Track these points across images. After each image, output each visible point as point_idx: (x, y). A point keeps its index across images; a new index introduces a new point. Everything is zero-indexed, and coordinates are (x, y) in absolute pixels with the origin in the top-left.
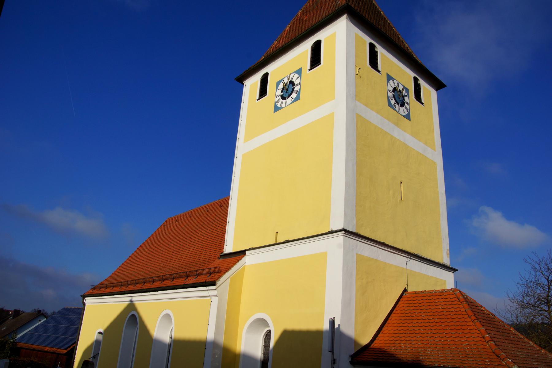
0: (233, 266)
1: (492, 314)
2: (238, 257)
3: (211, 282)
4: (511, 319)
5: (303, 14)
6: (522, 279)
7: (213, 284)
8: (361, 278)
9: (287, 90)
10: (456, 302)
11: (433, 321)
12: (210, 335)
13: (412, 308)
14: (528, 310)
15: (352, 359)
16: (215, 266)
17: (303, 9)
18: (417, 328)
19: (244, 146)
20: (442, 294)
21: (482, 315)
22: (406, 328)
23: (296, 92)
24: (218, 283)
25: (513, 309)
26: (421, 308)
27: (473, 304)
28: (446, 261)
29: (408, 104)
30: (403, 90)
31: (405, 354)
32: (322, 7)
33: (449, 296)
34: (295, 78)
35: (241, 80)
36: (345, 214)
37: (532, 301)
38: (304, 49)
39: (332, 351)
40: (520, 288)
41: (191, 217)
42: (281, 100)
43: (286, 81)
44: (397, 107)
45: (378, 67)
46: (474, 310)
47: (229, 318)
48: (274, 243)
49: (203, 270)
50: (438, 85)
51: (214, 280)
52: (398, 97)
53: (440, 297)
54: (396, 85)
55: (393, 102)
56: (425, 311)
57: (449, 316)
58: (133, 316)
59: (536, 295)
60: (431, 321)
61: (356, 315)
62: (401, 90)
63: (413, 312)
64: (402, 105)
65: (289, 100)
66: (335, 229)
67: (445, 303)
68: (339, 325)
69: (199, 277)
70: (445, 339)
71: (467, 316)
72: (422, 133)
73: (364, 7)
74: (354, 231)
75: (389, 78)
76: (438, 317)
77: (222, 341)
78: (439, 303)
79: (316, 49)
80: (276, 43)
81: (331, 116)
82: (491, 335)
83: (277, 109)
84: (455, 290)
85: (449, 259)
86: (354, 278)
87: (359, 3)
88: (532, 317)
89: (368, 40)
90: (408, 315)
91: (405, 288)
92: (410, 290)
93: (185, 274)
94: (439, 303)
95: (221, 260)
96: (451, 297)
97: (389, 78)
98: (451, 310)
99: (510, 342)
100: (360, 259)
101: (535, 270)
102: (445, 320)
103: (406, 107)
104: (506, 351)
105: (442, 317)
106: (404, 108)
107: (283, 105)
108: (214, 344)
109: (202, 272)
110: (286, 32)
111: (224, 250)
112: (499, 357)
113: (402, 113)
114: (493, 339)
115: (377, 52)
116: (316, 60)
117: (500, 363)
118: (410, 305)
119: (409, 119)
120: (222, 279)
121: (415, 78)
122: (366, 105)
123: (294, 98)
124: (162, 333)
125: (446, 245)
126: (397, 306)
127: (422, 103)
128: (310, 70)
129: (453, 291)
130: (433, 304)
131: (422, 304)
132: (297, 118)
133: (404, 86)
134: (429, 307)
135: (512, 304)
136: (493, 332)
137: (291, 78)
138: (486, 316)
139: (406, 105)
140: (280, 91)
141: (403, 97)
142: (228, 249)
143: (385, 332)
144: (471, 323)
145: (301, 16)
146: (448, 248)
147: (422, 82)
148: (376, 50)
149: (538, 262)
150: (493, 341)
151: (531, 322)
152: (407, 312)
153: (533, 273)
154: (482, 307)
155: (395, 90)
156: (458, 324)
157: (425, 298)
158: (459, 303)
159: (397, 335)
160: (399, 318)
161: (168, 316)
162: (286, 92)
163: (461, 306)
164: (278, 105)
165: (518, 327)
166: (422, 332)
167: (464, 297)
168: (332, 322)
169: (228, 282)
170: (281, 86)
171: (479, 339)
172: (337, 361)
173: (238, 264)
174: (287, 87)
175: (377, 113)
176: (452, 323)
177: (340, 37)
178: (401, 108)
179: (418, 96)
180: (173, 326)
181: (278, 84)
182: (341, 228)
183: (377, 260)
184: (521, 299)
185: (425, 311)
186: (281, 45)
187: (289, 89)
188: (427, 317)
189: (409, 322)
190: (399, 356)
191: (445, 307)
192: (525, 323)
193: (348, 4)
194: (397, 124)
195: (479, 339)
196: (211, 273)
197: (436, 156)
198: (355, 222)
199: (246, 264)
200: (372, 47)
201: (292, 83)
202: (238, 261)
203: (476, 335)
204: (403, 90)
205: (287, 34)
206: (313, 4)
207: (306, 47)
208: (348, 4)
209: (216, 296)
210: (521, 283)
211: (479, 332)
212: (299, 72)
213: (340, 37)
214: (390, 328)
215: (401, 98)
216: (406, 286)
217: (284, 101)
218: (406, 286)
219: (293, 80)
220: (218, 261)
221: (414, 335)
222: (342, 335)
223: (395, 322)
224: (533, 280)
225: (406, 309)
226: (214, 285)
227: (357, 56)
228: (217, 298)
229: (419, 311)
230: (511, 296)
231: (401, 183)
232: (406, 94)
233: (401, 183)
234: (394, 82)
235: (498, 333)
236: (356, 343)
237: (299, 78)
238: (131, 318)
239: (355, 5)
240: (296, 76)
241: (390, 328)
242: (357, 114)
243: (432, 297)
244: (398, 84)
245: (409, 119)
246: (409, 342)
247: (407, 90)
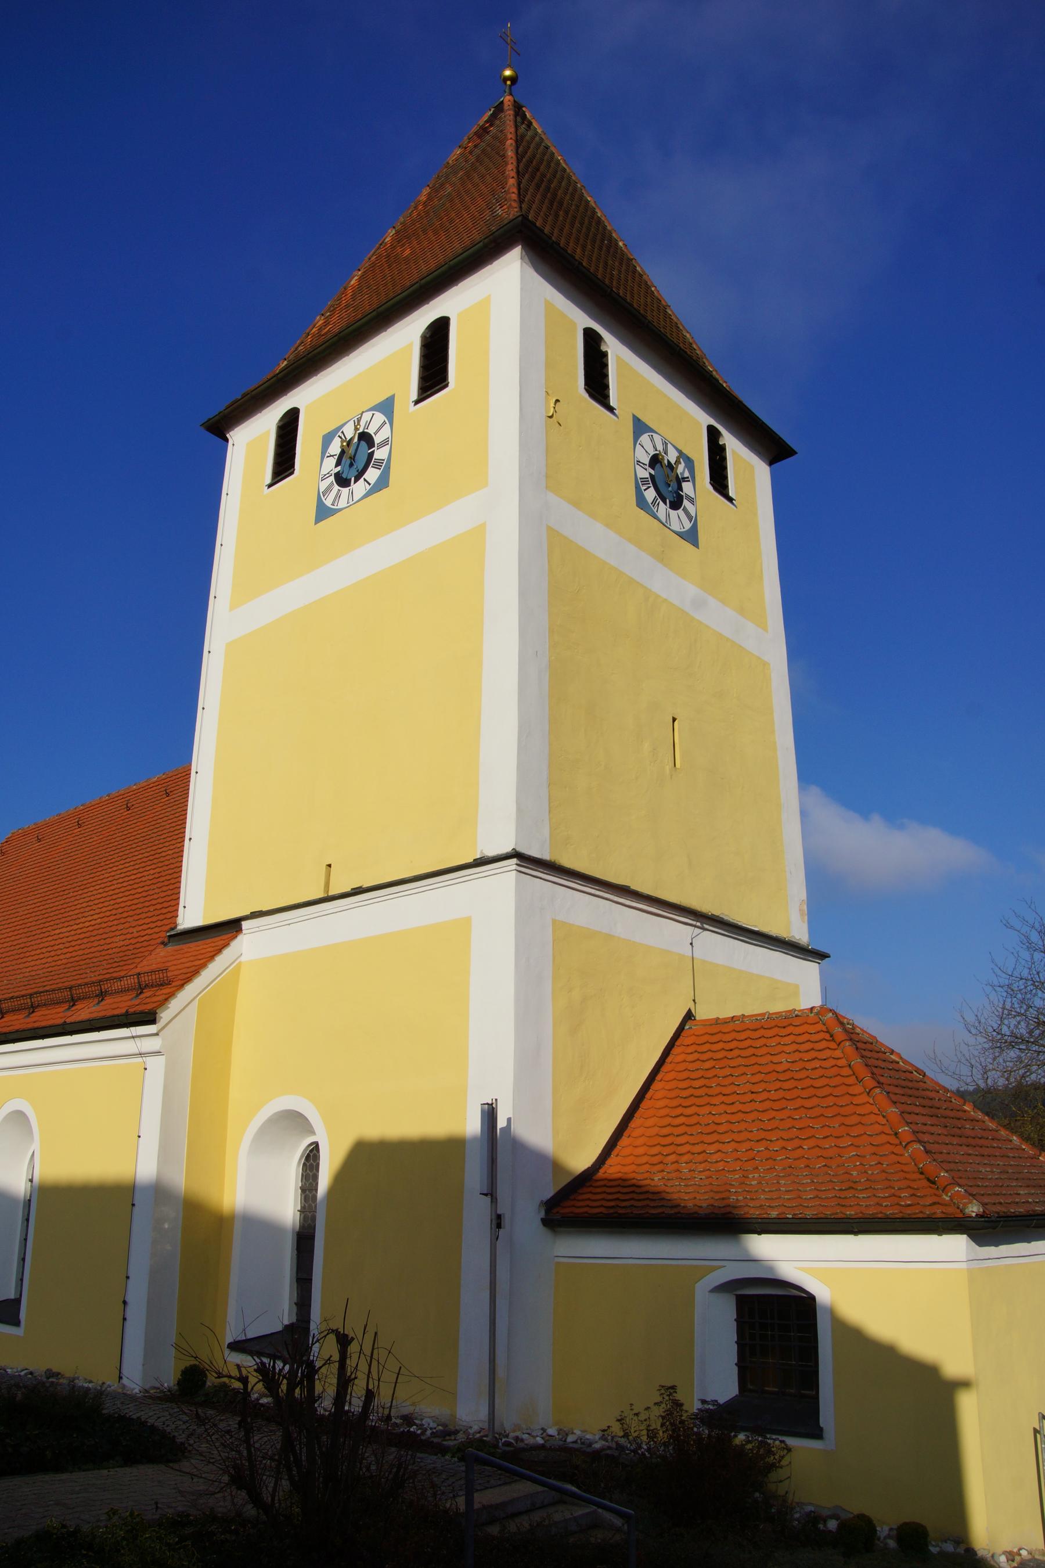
0: (204, 966)
1: (918, 1070)
2: (218, 941)
3: (142, 1013)
4: (969, 1080)
5: (403, 236)
6: (999, 973)
7: (149, 1018)
8: (566, 987)
9: (353, 459)
10: (824, 1044)
11: (765, 1095)
12: (145, 1166)
13: (707, 1065)
14: (1013, 1054)
15: (547, 1212)
16: (154, 967)
17: (399, 227)
18: (723, 1119)
19: (233, 617)
20: (787, 1023)
21: (892, 1073)
22: (694, 1120)
23: (377, 466)
24: (165, 1016)
25: (976, 1053)
26: (733, 1063)
27: (868, 1046)
28: (800, 934)
29: (692, 501)
30: (678, 462)
31: (691, 1189)
32: (451, 221)
33: (805, 1028)
34: (375, 423)
35: (220, 428)
36: (519, 810)
37: (1023, 1030)
38: (402, 341)
39: (491, 1194)
40: (993, 996)
41: (39, 840)
42: (336, 487)
43: (349, 432)
44: (662, 509)
45: (608, 396)
46: (871, 1062)
47: (200, 1115)
48: (321, 895)
49: (120, 978)
50: (774, 449)
51: (149, 1007)
52: (665, 483)
53: (783, 1032)
54: (660, 447)
55: (650, 494)
56: (742, 1070)
57: (807, 1083)
59: (1032, 1013)
60: (759, 1098)
62: (673, 462)
63: (710, 1074)
64: (676, 504)
65: (359, 488)
66: (491, 853)
67: (795, 1047)
68: (509, 1120)
69: (108, 1000)
70: (796, 1143)
71: (852, 1080)
72: (728, 579)
73: (572, 225)
74: (546, 856)
75: (640, 428)
76: (778, 1084)
77: (179, 1180)
78: (780, 1048)
79: (436, 343)
80: (320, 321)
81: (478, 535)
82: (913, 1126)
83: (323, 513)
84: (823, 1010)
85: (805, 926)
87: (557, 216)
88: (1021, 1072)
89: (581, 320)
90: (697, 1084)
91: (690, 1011)
92: (702, 1013)
93: (95, 989)
94: (780, 1048)
95: (170, 948)
96: (812, 1029)
97: (640, 428)
98: (809, 1065)
99: (963, 1140)
100: (564, 935)
101: (1030, 947)
102: (795, 1093)
103: (685, 510)
104: (952, 1166)
105: (786, 1085)
106: (680, 511)
107: (342, 503)
108: (159, 1191)
109: (117, 985)
110: (349, 292)
111: (180, 920)
112: (934, 1183)
113: (676, 526)
114: (920, 1135)
115: (605, 355)
116: (433, 374)
117: (934, 1199)
118: (704, 1057)
119: (695, 543)
121: (711, 430)
122: (576, 504)
123: (372, 481)
125: (797, 890)
126: (669, 1060)
127: (730, 500)
128: (417, 402)
129: (818, 1014)
130: (764, 1050)
131: (736, 1052)
132: (381, 542)
133: (680, 452)
134: (753, 1060)
135: (971, 1040)
136: (920, 1119)
137: (363, 423)
138: (903, 1076)
139: (686, 502)
140: (333, 461)
141: (679, 481)
142: (192, 914)
143: (637, 1133)
144: (864, 1098)
145: (393, 247)
146: (804, 895)
147: (730, 441)
148: (603, 348)
149: (1037, 925)
150: (920, 1142)
151: (1020, 1083)
152: (694, 1075)
153: (1025, 955)
154: (892, 1052)
155: (655, 461)
156: (830, 1101)
157: (743, 1036)
158: (833, 1045)
159: (668, 1140)
160: (673, 1094)
161: (19, 1117)
162: (351, 465)
163: (838, 1053)
164: (328, 502)
165: (988, 1100)
166: (736, 1127)
167: (845, 1030)
168: (490, 1113)
170: (335, 448)
171: (883, 1138)
172: (506, 1221)
173: (219, 959)
174: (351, 451)
175: (607, 525)
176: (815, 1101)
177: (502, 306)
178: (673, 513)
179: (719, 480)
180: (36, 1146)
181: (327, 440)
182: (507, 849)
184: (995, 1026)
185: (742, 1070)
186: (336, 330)
187: (356, 458)
188: (749, 1086)
189: (698, 1101)
190: (675, 1196)
191: (796, 1056)
192: (1006, 1086)
193: (525, 217)
194: (662, 557)
195: (883, 1138)
196: (141, 989)
197: (767, 641)
198: (546, 832)
199: (243, 959)
200: (591, 339)
201: (366, 438)
202: (219, 951)
203: (878, 1128)
204: (678, 462)
205: (354, 298)
206: (427, 213)
207: (406, 336)
208: (525, 217)
209: (158, 1053)
210: (996, 983)
211: (884, 1121)
212: (387, 407)
213: (502, 306)
214: (650, 1122)
215: (674, 485)
216: (691, 1005)
217: (345, 491)
218: (691, 1005)
219: (371, 430)
220: (162, 952)
221: (714, 1137)
222: (518, 1146)
223: (662, 1103)
224: (1025, 973)
225: (691, 1067)
226: (152, 1021)
227: (549, 365)
228: (161, 1060)
229: (727, 1071)
230: (971, 1018)
231: (674, 720)
232: (687, 474)
233: (674, 720)
234: (652, 439)
235: (934, 1120)
236: (557, 1167)
237: (388, 426)
239: (545, 221)
240: (379, 418)
241: (650, 1122)
242: (549, 529)
243: (748, 1034)
244: (665, 444)
245: (695, 543)
246: (700, 1158)
247: (690, 463)
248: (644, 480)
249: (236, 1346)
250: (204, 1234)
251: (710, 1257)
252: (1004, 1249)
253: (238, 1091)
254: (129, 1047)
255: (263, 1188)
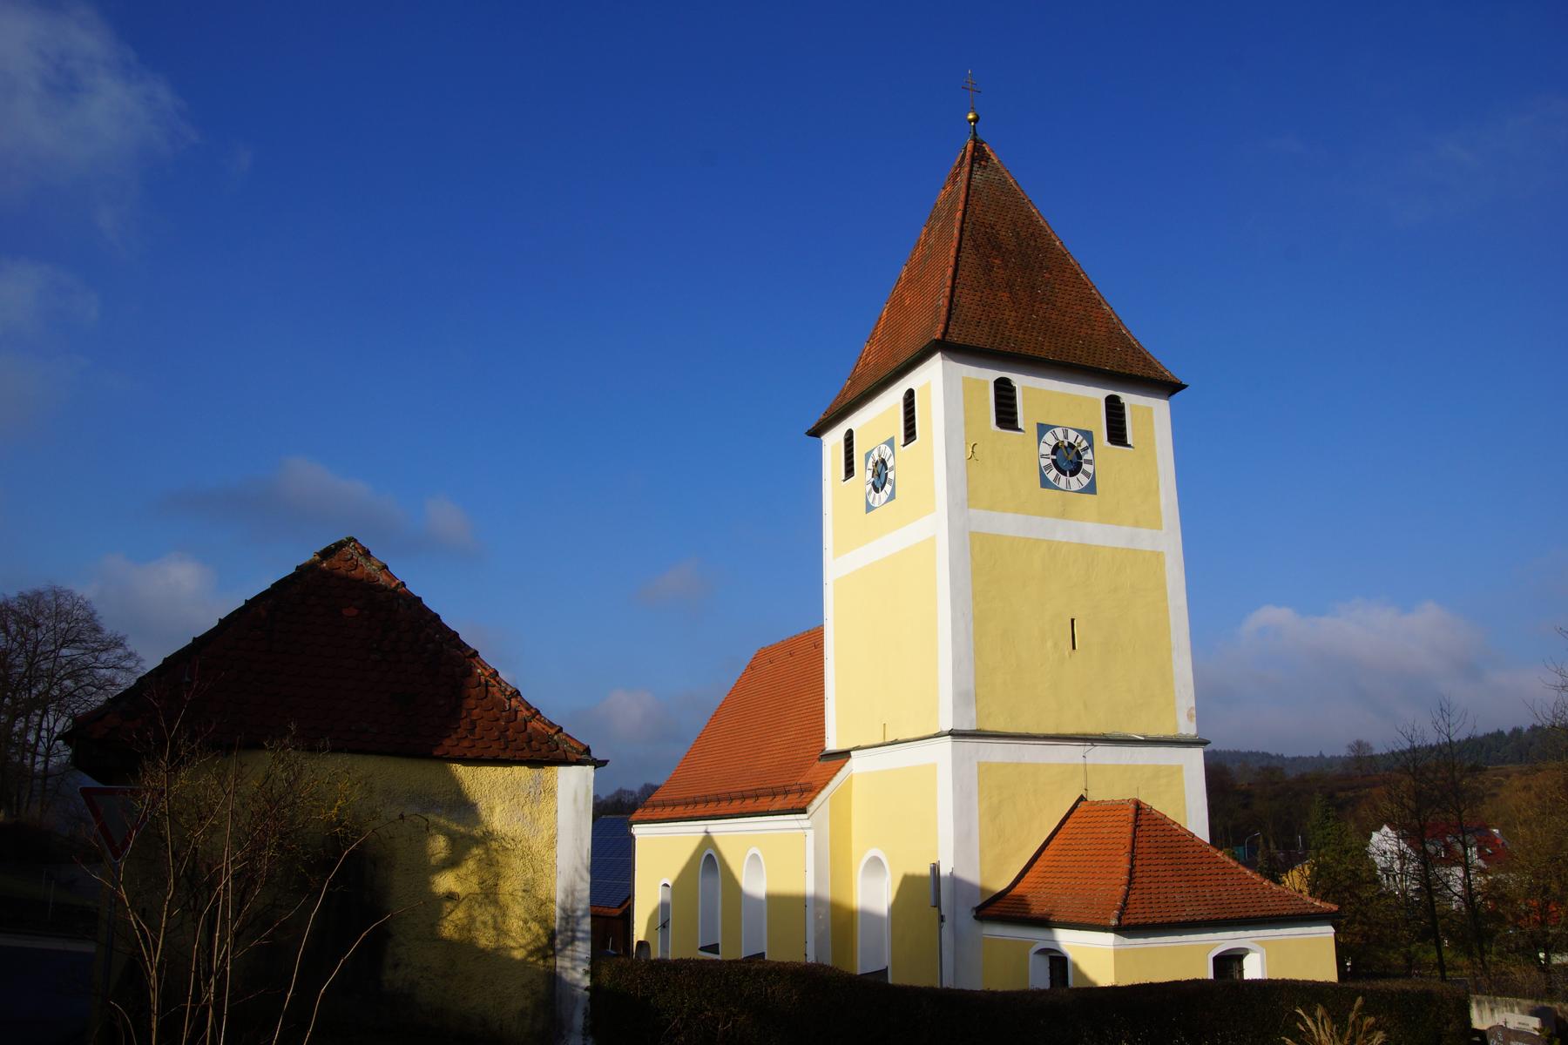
7: (803, 811)
12: (809, 888)
24: (811, 809)
35: (818, 432)
47: (836, 856)
58: (710, 856)
61: (981, 851)
77: (827, 893)
86: (976, 798)
92: (1093, 796)
100: (985, 769)
108: (817, 900)
120: (816, 802)
124: (755, 884)
139: (1085, 466)
142: (832, 745)
146: (1193, 704)
155: (1056, 449)
161: (755, 856)
169: (827, 803)
181: (868, 455)
182: (947, 727)
183: (1018, 764)
194: (1063, 514)
198: (974, 714)
207: (892, 398)
220: (818, 764)
238: (709, 861)
248: (1047, 467)
249: (702, 949)
250: (842, 921)
251: (1035, 937)
252: (1184, 938)
253: (856, 845)
254: (796, 824)
255: (874, 895)
